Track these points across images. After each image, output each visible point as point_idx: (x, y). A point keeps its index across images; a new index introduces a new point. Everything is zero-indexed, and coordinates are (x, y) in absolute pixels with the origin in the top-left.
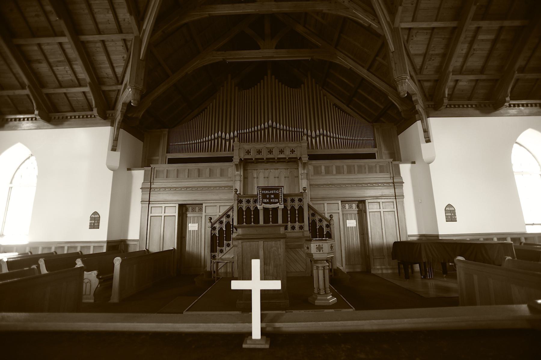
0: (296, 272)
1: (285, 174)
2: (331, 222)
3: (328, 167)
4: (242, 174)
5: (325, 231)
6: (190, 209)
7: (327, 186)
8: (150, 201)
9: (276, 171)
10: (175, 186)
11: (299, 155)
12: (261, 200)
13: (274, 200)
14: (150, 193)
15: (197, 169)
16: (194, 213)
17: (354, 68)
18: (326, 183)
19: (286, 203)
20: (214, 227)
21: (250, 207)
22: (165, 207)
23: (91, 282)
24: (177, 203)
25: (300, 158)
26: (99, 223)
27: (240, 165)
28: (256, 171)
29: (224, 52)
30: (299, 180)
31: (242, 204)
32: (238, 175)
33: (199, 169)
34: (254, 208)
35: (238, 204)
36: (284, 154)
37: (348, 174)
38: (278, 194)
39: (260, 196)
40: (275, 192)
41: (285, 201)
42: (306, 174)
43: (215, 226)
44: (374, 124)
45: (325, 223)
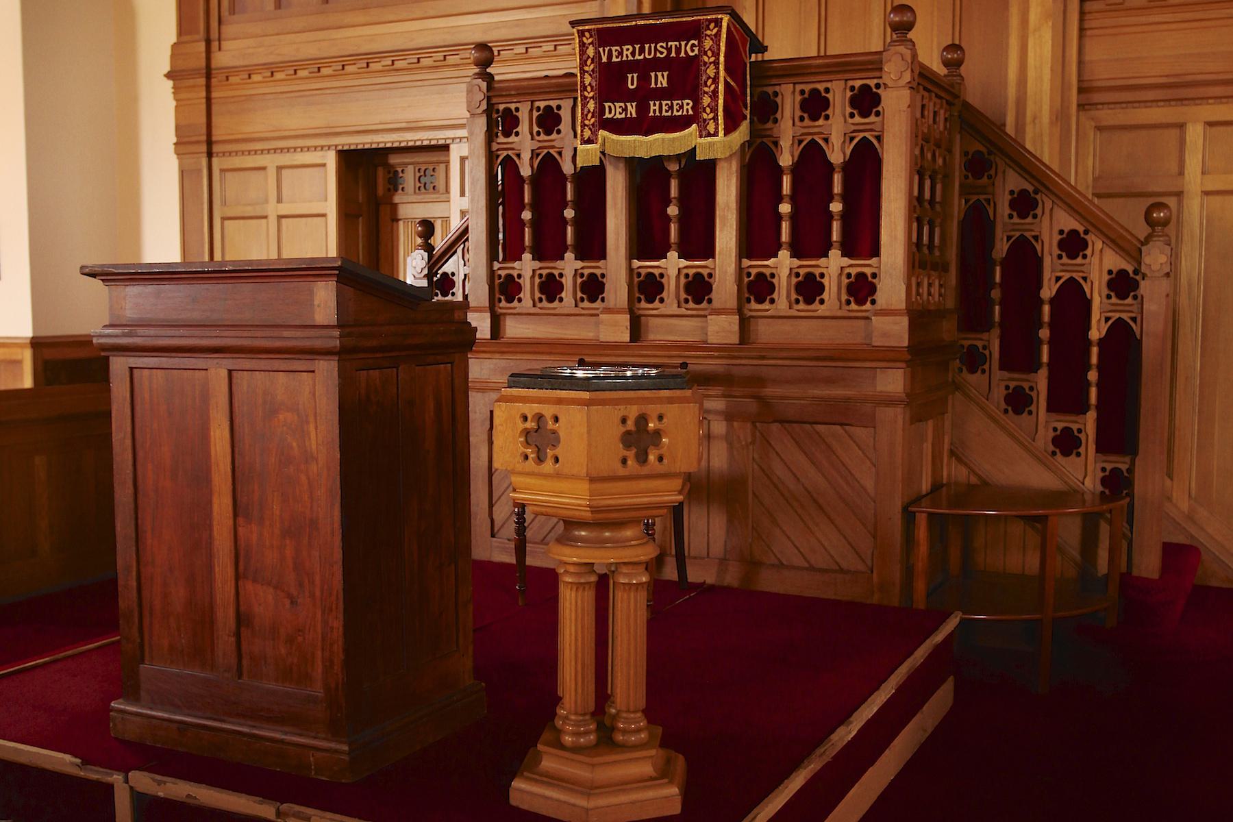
2: (1147, 259)
6: (409, 178)
8: (214, 139)
10: (310, 51)
12: (591, 105)
13: (671, 107)
16: (428, 197)
20: (445, 274)
21: (560, 153)
22: (280, 168)
24: (329, 147)
35: (490, 136)
38: (693, 65)
39: (588, 79)
43: (448, 267)
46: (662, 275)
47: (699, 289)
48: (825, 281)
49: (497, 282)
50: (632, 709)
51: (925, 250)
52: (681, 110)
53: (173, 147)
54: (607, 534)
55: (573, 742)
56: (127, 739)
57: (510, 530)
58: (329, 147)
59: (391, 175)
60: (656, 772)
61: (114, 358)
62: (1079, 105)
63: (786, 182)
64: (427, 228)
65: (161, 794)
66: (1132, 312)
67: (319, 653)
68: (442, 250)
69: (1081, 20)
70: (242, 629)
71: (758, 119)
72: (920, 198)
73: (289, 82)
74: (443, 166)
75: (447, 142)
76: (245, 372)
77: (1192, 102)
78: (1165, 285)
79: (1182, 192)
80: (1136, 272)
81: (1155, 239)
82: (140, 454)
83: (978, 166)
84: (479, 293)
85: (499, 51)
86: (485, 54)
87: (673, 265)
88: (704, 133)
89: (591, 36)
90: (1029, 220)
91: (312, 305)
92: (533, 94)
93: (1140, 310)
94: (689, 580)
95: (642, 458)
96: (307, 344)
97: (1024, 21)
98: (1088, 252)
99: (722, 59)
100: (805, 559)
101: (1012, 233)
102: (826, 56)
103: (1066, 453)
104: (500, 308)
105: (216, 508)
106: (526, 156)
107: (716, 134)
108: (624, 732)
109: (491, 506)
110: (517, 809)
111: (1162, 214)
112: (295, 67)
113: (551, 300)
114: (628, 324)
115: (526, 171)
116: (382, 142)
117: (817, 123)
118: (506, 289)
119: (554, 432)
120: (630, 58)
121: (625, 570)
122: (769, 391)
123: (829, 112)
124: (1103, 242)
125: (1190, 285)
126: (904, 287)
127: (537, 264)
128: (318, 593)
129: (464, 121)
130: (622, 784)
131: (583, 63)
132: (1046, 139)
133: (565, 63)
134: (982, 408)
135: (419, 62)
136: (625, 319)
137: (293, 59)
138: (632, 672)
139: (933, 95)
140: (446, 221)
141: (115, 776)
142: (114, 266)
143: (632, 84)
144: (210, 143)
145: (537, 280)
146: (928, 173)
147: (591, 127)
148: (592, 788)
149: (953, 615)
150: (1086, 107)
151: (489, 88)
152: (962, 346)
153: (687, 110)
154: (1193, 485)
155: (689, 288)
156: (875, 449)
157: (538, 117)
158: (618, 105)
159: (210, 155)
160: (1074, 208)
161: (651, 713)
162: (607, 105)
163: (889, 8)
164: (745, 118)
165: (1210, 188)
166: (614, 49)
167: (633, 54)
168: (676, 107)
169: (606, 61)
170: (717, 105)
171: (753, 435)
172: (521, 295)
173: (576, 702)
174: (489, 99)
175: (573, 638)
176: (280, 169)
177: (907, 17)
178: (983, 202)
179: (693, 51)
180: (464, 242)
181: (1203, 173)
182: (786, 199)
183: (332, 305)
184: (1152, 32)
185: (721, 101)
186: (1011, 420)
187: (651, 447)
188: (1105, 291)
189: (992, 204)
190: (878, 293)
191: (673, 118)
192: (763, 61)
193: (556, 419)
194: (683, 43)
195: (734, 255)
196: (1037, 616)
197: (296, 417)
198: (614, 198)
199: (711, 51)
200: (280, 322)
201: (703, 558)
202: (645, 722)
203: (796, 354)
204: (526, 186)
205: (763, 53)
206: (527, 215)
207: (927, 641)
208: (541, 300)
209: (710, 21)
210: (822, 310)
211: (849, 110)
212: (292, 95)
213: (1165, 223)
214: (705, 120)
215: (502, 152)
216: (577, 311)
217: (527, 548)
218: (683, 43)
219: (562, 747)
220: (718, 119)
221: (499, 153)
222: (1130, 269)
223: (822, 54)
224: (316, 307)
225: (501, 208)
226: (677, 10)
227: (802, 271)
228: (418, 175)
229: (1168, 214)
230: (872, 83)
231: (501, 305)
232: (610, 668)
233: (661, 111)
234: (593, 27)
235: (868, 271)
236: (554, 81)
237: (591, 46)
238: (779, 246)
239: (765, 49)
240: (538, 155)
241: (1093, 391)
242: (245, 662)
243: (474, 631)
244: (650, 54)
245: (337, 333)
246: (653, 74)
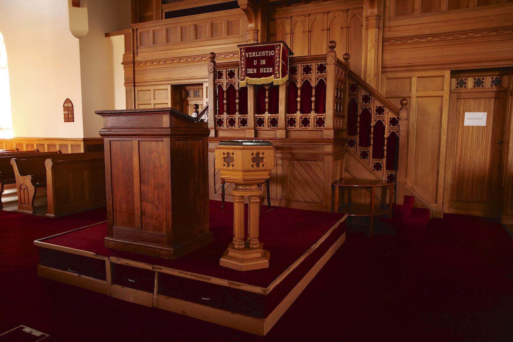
0: (306, 202)
2: (401, 115)
4: (259, 28)
5: (386, 131)
6: (192, 93)
7: (476, 35)
8: (136, 82)
10: (163, 56)
12: (243, 70)
13: (266, 70)
14: (134, 70)
15: (193, 25)
21: (234, 84)
22: (154, 90)
23: (28, 189)
26: (73, 114)
28: (289, 21)
35: (214, 79)
39: (242, 62)
40: (268, 54)
45: (388, 116)
46: (263, 119)
47: (274, 122)
48: (310, 120)
49: (217, 121)
50: (255, 238)
51: (338, 112)
53: (124, 84)
54: (248, 187)
55: (238, 247)
56: (109, 248)
57: (220, 192)
59: (187, 92)
60: (261, 256)
61: (105, 138)
62: (382, 72)
63: (299, 92)
64: (197, 106)
65: (119, 263)
66: (396, 130)
67: (165, 222)
68: (201, 112)
69: (383, 48)
70: (143, 216)
71: (291, 74)
72: (337, 97)
73: (157, 65)
74: (201, 90)
76: (143, 142)
77: (413, 71)
78: (406, 122)
79: (411, 97)
80: (398, 118)
81: (403, 109)
82: (113, 166)
83: (353, 88)
84: (211, 125)
85: (217, 56)
86: (213, 55)
87: (267, 116)
89: (243, 50)
90: (368, 103)
91: (162, 122)
92: (227, 67)
93: (399, 129)
94: (271, 205)
95: (258, 165)
96: (161, 133)
97: (367, 47)
98: (384, 113)
99: (281, 56)
100: (304, 199)
101: (363, 107)
102: (310, 56)
103: (378, 170)
104: (218, 128)
105: (135, 181)
106: (225, 85)
107: (279, 78)
108: (252, 244)
109: (215, 184)
110: (222, 266)
111: (405, 102)
112: (159, 61)
113: (232, 126)
114: (254, 132)
115: (225, 89)
116: (184, 83)
117: (308, 75)
118: (219, 123)
119: (232, 158)
120: (255, 56)
121: (253, 198)
122: (294, 151)
123: (311, 72)
124: (389, 110)
125: (412, 123)
126: (332, 122)
127: (228, 116)
128: (164, 205)
129: (207, 77)
130: (252, 259)
131: (241, 57)
132: (372, 82)
133: (236, 59)
134: (354, 157)
135: (194, 60)
136: (253, 131)
137: (158, 59)
138: (255, 227)
139: (341, 67)
140: (202, 105)
141: (106, 258)
142: (104, 111)
143: (255, 63)
144: (134, 83)
145: (228, 120)
146: (339, 90)
148: (243, 260)
149: (346, 215)
150: (384, 72)
152: (349, 140)
153: (271, 71)
154: (413, 180)
155: (271, 122)
156: (324, 168)
157: (228, 73)
158: (251, 69)
159: (134, 86)
160: (380, 100)
161: (260, 239)
162: (248, 69)
163: (328, 42)
164: (288, 74)
165: (418, 95)
166: (250, 53)
167: (255, 55)
168: (268, 70)
170: (279, 70)
171: (289, 164)
172: (223, 124)
173: (239, 236)
174: (214, 68)
175: (238, 217)
177: (334, 44)
178: (355, 99)
179: (272, 54)
180: (207, 110)
181: (416, 91)
182: (299, 97)
183: (168, 122)
184: (403, 51)
185: (281, 68)
186: (362, 160)
187: (260, 162)
188: (389, 124)
189: (357, 99)
190: (325, 123)
191: (267, 73)
192: (292, 57)
193: (233, 154)
194: (270, 52)
195: (284, 112)
196: (369, 215)
197: (158, 154)
198: (250, 96)
200: (153, 127)
201: (275, 199)
202: (259, 241)
203: (301, 141)
204: (225, 93)
205: (292, 55)
206: (225, 102)
207: (339, 221)
208: (229, 126)
209: (278, 45)
210: (309, 128)
211: (317, 71)
212: (158, 69)
213: (406, 104)
214: (276, 74)
216: (239, 129)
217: (225, 197)
218: (270, 52)
219: (235, 249)
221: (217, 84)
222: (396, 117)
223: (309, 55)
224: (164, 123)
225: (218, 100)
226: (268, 42)
227: (303, 117)
228: (194, 92)
229: (407, 102)
230: (324, 63)
231: (218, 127)
232: (248, 227)
233: (263, 71)
234: (244, 47)
235: (322, 117)
236: (233, 63)
238: (297, 110)
239: (293, 54)
240: (228, 84)
241: (385, 152)
242: (143, 225)
243: (210, 219)
244: (260, 55)
245: (170, 130)
246: (261, 61)
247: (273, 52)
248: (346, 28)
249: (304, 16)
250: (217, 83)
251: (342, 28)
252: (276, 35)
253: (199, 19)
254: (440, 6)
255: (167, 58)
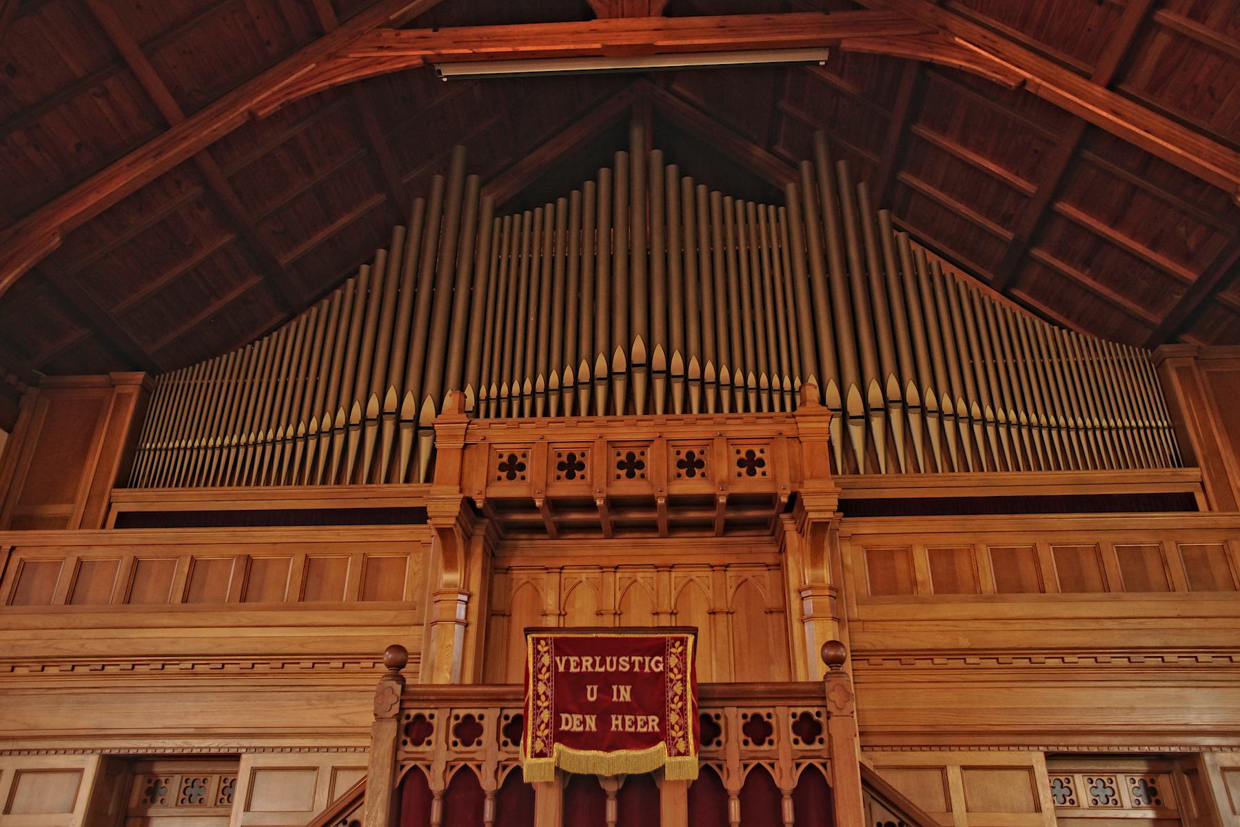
1: (710, 593)
3: (950, 553)
4: (475, 587)
6: (173, 788)
7: (952, 663)
9: (665, 576)
10: (100, 648)
11: (788, 483)
12: (546, 716)
13: (635, 723)
16: (191, 810)
17: (1038, 80)
18: (943, 642)
19: (713, 747)
21: (479, 767)
24: (93, 750)
25: (794, 498)
27: (468, 538)
28: (554, 578)
29: (428, 32)
30: (787, 629)
31: (428, 749)
32: (451, 587)
33: (249, 561)
34: (502, 777)
35: (397, 745)
36: (703, 475)
37: (1064, 596)
38: (659, 679)
41: (708, 731)
42: (831, 588)
44: (1165, 348)
52: (646, 726)
58: (93, 750)
75: (239, 751)
86: (400, 657)
88: (673, 752)
89: (547, 644)
106: (439, 768)
120: (590, 669)
137: (75, 654)
143: (592, 695)
147: (545, 739)
151: (403, 691)
158: (576, 717)
162: (564, 716)
166: (572, 659)
167: (593, 665)
168: (640, 723)
169: (563, 670)
176: (335, 770)
179: (657, 667)
181: (967, 811)
191: (636, 735)
194: (647, 659)
199: (677, 668)
209: (676, 639)
214: (673, 738)
215: (408, 762)
218: (647, 659)
220: (687, 738)
221: (405, 763)
228: (184, 785)
233: (623, 726)
237: (547, 654)
240: (452, 767)
246: (615, 688)
247: (657, 662)
248: (667, 613)
249: (600, 570)
250: (405, 760)
251: (714, 613)
252: (510, 615)
253: (266, 540)
254: (976, 580)
255: (115, 653)
